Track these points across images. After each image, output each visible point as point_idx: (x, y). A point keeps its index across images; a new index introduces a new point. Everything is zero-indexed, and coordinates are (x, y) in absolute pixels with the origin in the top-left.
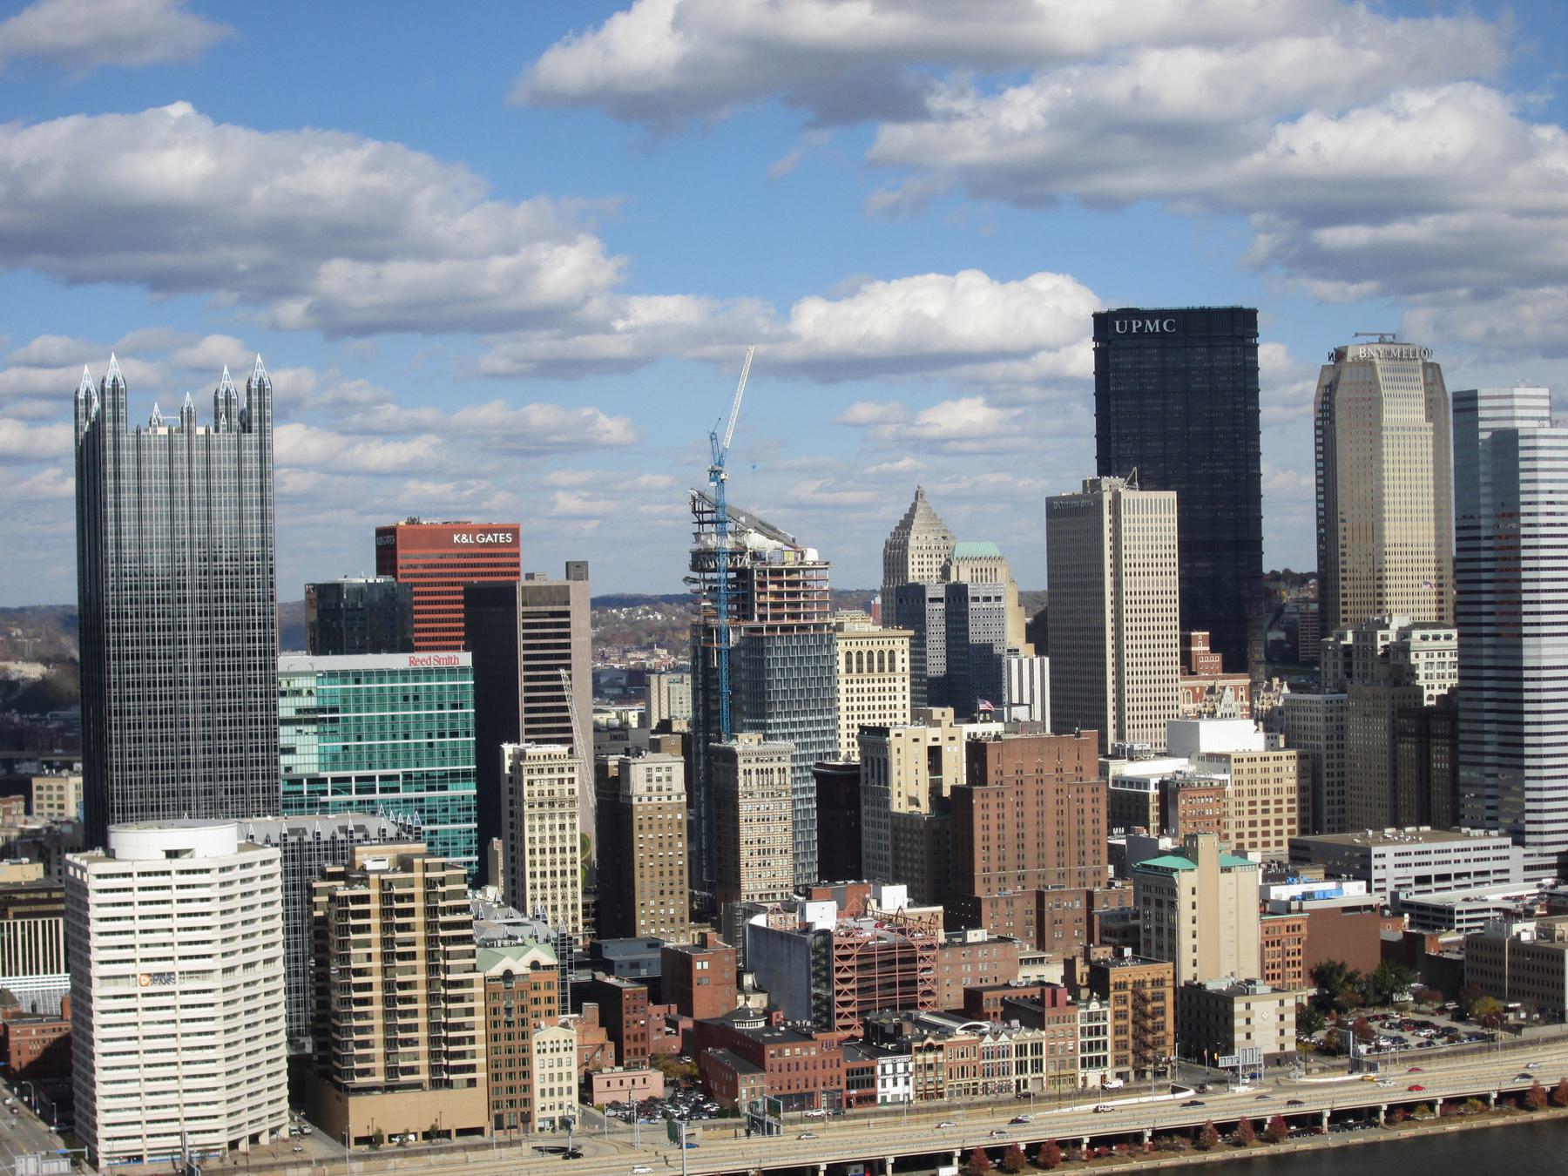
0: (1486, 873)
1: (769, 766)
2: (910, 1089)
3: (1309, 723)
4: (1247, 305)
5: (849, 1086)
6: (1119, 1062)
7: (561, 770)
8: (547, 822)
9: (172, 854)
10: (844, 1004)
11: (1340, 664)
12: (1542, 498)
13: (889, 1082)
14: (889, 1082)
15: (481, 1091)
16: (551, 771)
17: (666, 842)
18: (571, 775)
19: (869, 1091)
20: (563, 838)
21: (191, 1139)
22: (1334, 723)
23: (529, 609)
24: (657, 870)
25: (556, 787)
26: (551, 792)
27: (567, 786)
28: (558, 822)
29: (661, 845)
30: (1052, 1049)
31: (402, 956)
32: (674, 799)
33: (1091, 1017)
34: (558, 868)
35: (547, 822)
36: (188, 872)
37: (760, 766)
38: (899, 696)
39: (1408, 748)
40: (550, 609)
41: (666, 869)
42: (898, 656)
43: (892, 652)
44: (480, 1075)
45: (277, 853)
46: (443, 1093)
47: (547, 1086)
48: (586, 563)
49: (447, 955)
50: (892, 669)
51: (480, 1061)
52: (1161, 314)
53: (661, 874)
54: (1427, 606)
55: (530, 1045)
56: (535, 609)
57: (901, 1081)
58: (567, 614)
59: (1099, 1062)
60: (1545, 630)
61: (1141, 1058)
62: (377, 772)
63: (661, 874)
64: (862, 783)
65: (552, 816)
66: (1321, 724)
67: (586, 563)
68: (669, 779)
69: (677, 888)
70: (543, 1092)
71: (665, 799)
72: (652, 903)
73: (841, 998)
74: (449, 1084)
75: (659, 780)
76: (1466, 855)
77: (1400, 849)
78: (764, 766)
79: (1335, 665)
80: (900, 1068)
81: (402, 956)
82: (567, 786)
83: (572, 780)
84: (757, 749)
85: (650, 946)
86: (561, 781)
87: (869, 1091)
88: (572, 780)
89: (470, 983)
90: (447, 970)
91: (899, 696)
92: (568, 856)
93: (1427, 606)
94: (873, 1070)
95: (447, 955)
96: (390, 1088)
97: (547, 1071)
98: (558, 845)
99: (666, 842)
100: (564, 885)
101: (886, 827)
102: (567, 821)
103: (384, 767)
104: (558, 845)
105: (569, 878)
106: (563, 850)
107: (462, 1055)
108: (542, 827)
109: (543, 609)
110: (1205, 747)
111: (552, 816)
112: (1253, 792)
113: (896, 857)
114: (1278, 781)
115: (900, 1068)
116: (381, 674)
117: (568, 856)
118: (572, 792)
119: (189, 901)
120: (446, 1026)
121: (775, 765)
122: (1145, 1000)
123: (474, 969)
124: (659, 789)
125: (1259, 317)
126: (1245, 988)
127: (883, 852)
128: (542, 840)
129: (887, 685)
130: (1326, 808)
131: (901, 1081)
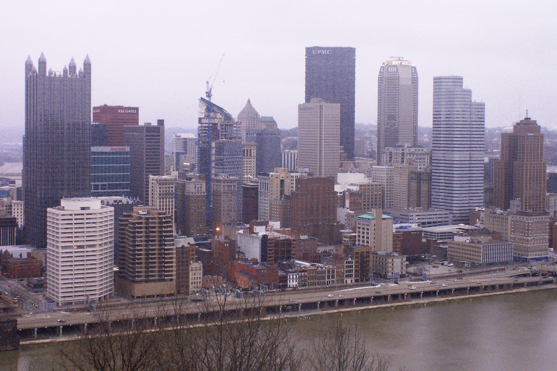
0: (442, 222)
1: (231, 184)
2: (296, 283)
3: (381, 175)
4: (353, 47)
5: (280, 282)
6: (356, 276)
7: (169, 184)
9: (83, 209)
10: (270, 257)
11: (388, 158)
12: (456, 109)
13: (291, 281)
14: (291, 281)
15: (174, 283)
16: (166, 184)
17: (200, 207)
19: (285, 283)
21: (90, 297)
22: (389, 175)
25: (168, 189)
26: (166, 191)
27: (171, 189)
30: (337, 272)
31: (152, 241)
33: (349, 262)
36: (89, 214)
38: (252, 163)
39: (414, 184)
42: (252, 151)
43: (251, 150)
44: (174, 277)
45: (112, 209)
46: (163, 283)
47: (193, 281)
49: (165, 241)
50: (250, 155)
51: (174, 273)
52: (327, 49)
55: (189, 269)
57: (295, 281)
58: (159, 136)
59: (350, 276)
60: (455, 149)
61: (362, 275)
62: (100, 183)
64: (259, 190)
66: (385, 175)
68: (201, 188)
70: (192, 283)
73: (270, 256)
74: (164, 280)
75: (198, 188)
76: (436, 216)
77: (417, 214)
78: (229, 184)
79: (387, 158)
80: (295, 277)
81: (152, 241)
82: (171, 189)
83: (172, 187)
86: (169, 187)
87: (285, 283)
88: (172, 187)
89: (172, 249)
90: (165, 245)
91: (252, 163)
94: (287, 277)
95: (165, 241)
96: (147, 281)
97: (193, 276)
99: (200, 207)
101: (267, 203)
103: (102, 182)
107: (169, 271)
108: (163, 202)
112: (368, 196)
113: (270, 213)
114: (372, 192)
115: (295, 277)
116: (102, 153)
118: (172, 191)
119: (89, 223)
120: (164, 262)
122: (364, 258)
123: (173, 245)
124: (198, 191)
125: (356, 50)
126: (388, 255)
127: (266, 211)
129: (249, 160)
130: (386, 201)
131: (295, 281)
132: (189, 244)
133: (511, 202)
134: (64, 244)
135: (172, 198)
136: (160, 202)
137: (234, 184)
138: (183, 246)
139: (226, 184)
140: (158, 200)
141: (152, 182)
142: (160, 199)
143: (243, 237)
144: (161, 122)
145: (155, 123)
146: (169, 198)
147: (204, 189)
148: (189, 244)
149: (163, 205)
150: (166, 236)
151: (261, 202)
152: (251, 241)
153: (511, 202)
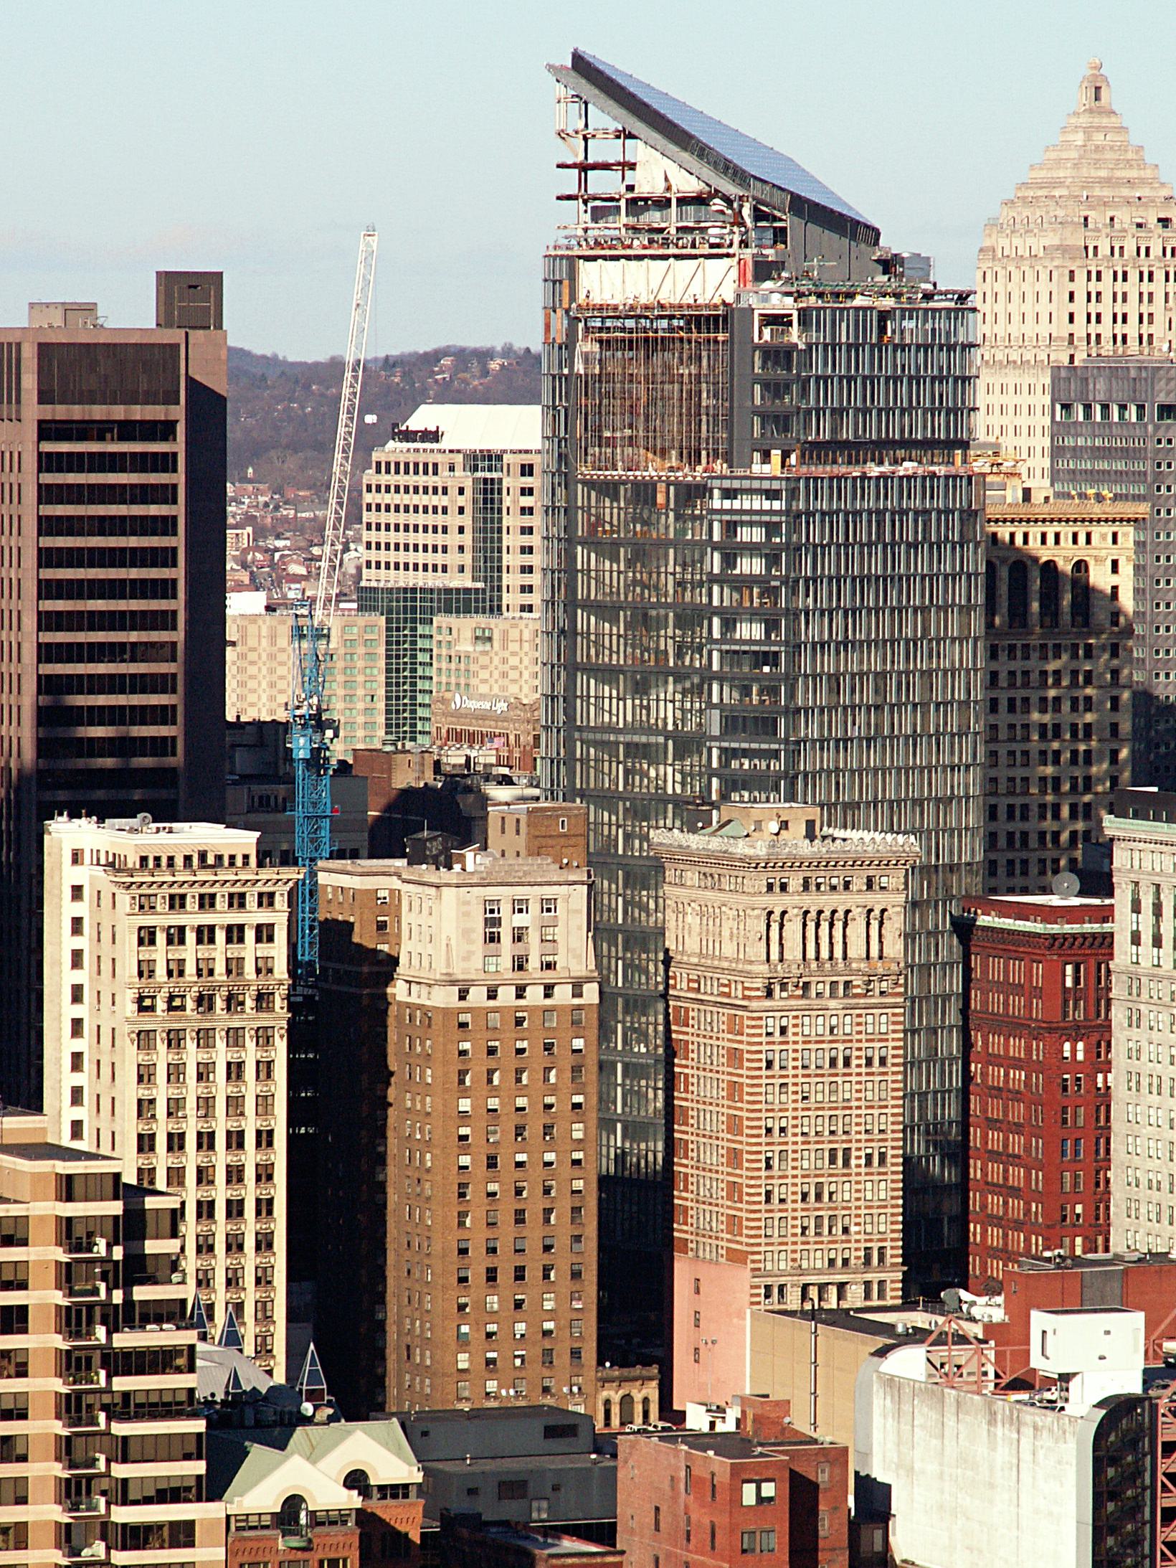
1: (840, 901)
7: (237, 901)
8: (192, 1055)
16: (207, 902)
18: (263, 917)
20: (234, 1104)
23: (60, 412)
24: (507, 1207)
27: (249, 949)
28: (221, 1054)
29: (519, 1131)
32: (563, 995)
34: (220, 1193)
35: (192, 1055)
37: (813, 901)
40: (119, 412)
41: (534, 1204)
48: (216, 279)
53: (520, 1217)
54: (1024, 399)
56: (76, 412)
63: (520, 1217)
65: (205, 1038)
67: (216, 279)
69: (562, 1261)
71: (535, 995)
72: (493, 1302)
78: (827, 901)
82: (249, 949)
84: (806, 849)
85: (552, 1432)
88: (264, 933)
92: (250, 1157)
93: (1024, 399)
98: (221, 1125)
100: (234, 1245)
102: (251, 1054)
104: (221, 1125)
105: (250, 1226)
106: (236, 1140)
108: (175, 1072)
109: (98, 412)
110: (378, 738)
111: (205, 1038)
117: (250, 1157)
121: (855, 900)
128: (175, 1107)
132: (356, 1480)
133: (355, 1492)
134: (757, 1107)
135: (263, 1036)
136: (145, 1075)
137: (877, 900)
138: (293, 1503)
139: (793, 901)
140: (130, 1057)
141: (80, 875)
142: (144, 1039)
143: (925, 1414)
144: (192, 296)
145: (131, 312)
146: (234, 1038)
147: (575, 951)
148: (356, 1480)
149: (175, 1107)
150: (126, 1408)
151: (1135, 1081)
152: (1003, 1454)
153: (355, 1492)
